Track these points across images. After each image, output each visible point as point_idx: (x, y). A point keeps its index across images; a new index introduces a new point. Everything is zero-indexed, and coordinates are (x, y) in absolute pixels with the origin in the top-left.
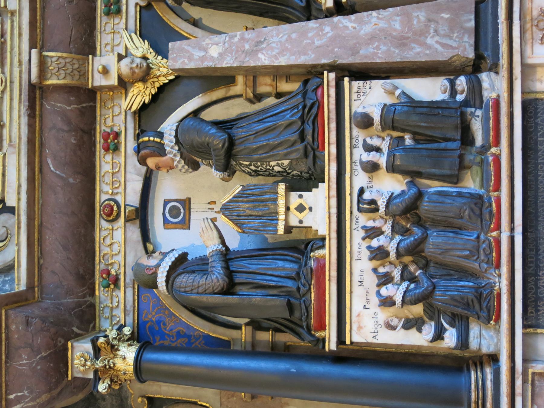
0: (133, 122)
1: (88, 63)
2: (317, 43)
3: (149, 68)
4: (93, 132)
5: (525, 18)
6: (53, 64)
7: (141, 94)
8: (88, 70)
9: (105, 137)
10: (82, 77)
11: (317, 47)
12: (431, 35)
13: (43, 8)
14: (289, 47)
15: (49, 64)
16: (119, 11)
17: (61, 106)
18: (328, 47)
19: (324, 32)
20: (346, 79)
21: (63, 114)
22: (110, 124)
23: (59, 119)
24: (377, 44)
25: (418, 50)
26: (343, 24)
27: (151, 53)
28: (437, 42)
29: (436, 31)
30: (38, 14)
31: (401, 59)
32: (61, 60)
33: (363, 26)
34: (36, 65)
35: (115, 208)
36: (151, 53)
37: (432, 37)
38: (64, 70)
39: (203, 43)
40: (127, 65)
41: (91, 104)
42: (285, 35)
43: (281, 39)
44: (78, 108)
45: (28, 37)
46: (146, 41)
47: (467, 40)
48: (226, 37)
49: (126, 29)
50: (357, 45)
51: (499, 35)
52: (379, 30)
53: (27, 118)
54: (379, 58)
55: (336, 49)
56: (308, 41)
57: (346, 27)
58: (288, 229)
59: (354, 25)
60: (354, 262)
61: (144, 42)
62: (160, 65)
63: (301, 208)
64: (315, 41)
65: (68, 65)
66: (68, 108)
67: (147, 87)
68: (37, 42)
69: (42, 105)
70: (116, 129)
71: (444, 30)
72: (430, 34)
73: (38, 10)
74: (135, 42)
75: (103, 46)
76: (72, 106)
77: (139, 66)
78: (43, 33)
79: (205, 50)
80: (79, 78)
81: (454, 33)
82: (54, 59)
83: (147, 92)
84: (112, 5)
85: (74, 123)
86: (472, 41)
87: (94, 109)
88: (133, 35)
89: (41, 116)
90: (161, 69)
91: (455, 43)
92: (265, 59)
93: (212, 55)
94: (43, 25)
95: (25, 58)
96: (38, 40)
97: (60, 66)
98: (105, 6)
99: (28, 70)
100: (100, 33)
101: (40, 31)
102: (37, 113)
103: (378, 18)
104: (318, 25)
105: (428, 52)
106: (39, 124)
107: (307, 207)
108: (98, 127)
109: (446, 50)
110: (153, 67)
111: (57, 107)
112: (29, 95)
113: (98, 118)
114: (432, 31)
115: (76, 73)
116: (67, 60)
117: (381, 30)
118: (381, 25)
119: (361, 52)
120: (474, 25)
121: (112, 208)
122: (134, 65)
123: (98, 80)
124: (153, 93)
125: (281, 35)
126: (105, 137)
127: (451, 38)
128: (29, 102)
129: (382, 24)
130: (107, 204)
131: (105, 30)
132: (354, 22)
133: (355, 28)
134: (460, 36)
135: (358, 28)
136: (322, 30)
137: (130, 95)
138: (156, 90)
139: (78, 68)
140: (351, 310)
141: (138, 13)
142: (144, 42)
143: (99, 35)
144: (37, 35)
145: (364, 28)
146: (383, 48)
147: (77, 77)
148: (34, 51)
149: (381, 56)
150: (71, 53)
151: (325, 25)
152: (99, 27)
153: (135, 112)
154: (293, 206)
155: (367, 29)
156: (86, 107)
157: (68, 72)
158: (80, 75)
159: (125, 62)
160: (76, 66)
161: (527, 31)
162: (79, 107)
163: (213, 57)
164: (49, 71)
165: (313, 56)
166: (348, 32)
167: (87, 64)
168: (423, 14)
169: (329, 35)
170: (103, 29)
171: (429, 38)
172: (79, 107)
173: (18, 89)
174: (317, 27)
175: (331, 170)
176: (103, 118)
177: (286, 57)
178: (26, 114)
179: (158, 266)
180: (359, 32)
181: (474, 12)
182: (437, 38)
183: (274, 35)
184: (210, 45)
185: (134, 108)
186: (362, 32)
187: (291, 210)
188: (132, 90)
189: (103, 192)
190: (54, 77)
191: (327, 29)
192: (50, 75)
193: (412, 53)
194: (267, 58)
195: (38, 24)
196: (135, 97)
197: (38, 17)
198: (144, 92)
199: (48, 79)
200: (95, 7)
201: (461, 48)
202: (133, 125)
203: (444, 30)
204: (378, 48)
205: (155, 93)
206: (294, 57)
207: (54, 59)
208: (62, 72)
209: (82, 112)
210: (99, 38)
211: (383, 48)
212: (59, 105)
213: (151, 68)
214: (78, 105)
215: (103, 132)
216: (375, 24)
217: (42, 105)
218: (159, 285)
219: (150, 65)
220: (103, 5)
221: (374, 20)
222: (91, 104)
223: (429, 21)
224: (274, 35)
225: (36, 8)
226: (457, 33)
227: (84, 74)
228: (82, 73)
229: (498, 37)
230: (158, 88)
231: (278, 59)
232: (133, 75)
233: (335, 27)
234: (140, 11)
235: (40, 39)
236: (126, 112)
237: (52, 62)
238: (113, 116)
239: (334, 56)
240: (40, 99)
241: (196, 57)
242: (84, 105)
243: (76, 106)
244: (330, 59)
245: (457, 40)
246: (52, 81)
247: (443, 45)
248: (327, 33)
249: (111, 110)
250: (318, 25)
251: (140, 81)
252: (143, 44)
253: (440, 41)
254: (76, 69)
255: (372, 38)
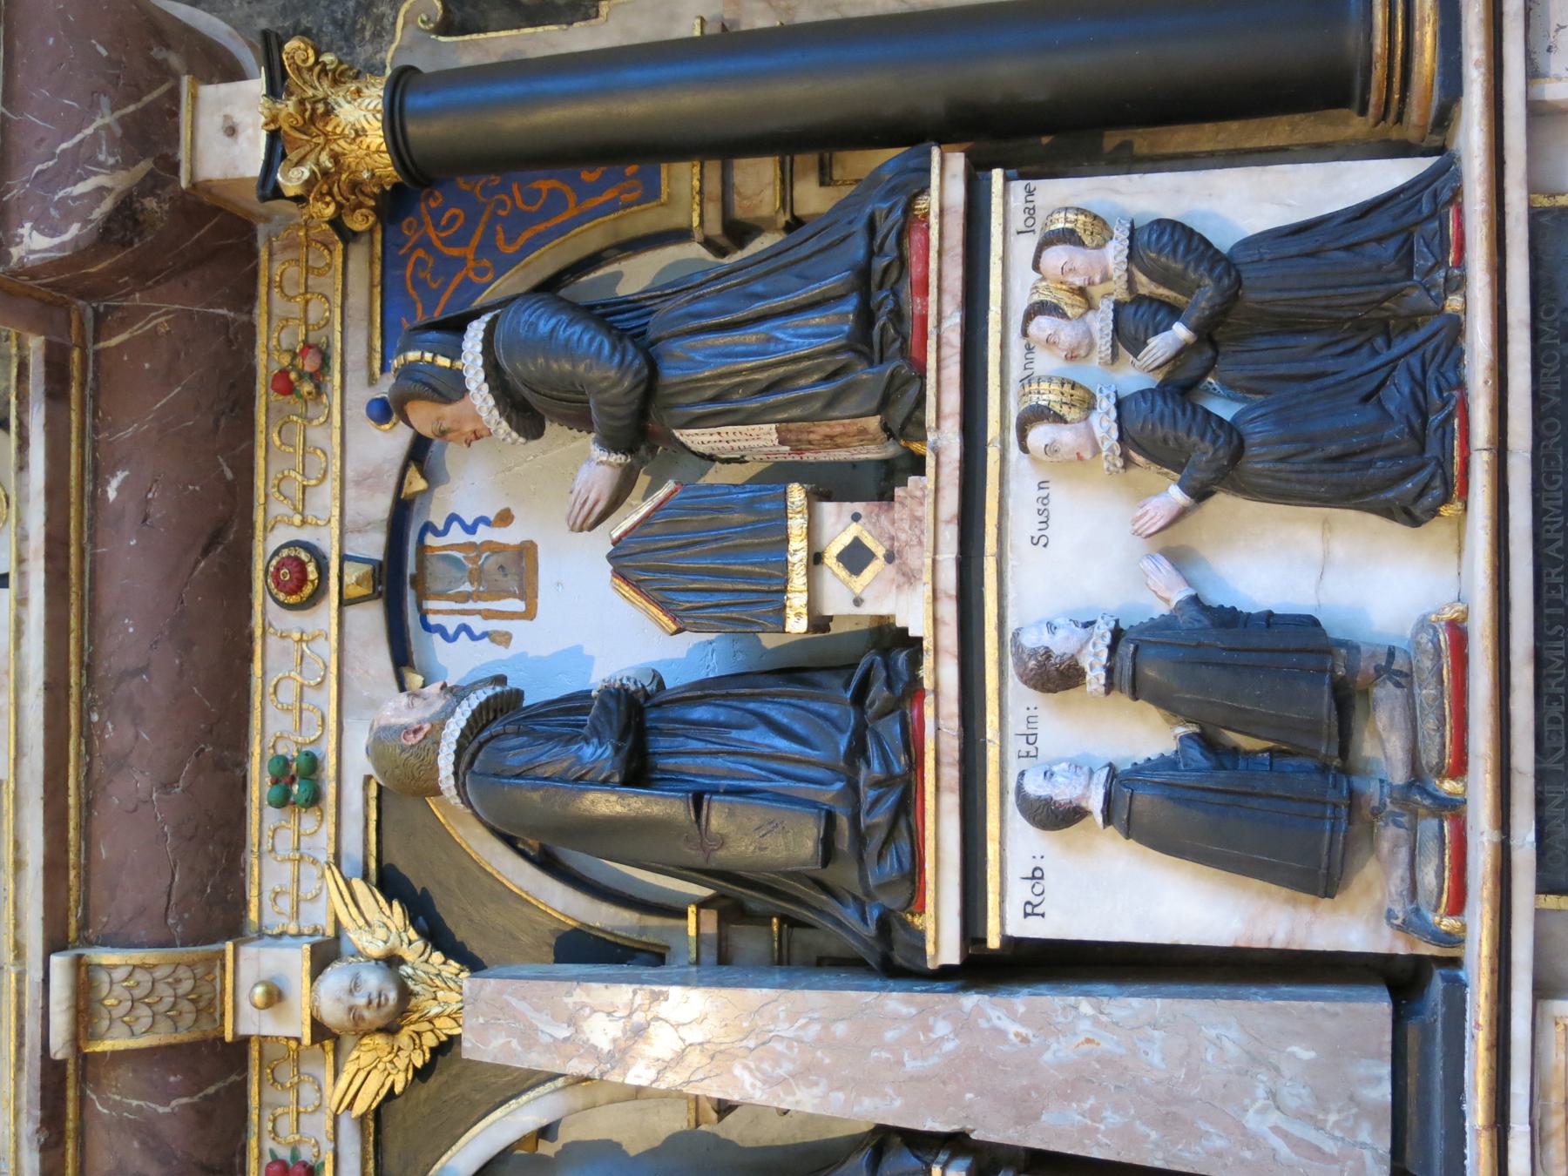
0: (357, 1137)
1: (223, 967)
2: (912, 1065)
3: (405, 994)
4: (237, 1161)
5: (1545, 1097)
6: (118, 990)
7: (381, 1066)
8: (223, 990)
9: (283, 774)
10: (204, 1014)
11: (911, 1078)
12: (1259, 1104)
13: (87, 806)
14: (827, 1061)
15: (105, 988)
16: (314, 799)
17: (140, 1107)
18: (944, 1083)
19: (933, 1036)
20: (997, 175)
21: (145, 1130)
22: (291, 1138)
23: (136, 1144)
24: (1092, 1101)
25: (1219, 1143)
26: (989, 1020)
27: (410, 943)
28: (1276, 1130)
29: (1272, 1095)
30: (72, 824)
31: (1167, 1162)
32: (140, 975)
33: (1052, 1040)
34: (65, 1006)
35: (312, 572)
36: (410, 943)
37: (1262, 1111)
38: (149, 1005)
39: (566, 1000)
40: (339, 1000)
41: (234, 1078)
42: (812, 1020)
43: (801, 1033)
44: (192, 1105)
45: (40, 913)
46: (396, 904)
47: (1369, 1141)
48: (635, 993)
49: (337, 856)
50: (1034, 1094)
51: (1467, 1151)
52: (1099, 1062)
53: (36, 1156)
54: (1099, 1144)
55: (969, 1096)
56: (885, 1055)
57: (1000, 1034)
58: (819, 623)
59: (1023, 1031)
60: (1013, 238)
61: (391, 906)
62: (438, 982)
63: (856, 557)
64: (906, 1058)
65: (161, 987)
66: (161, 1110)
67: (400, 1049)
68: (68, 909)
69: (82, 1100)
70: (307, 1154)
71: (1299, 1096)
72: (1254, 1101)
73: (72, 813)
74: (362, 905)
75: (267, 896)
76: (174, 1103)
77: (375, 1002)
78: (85, 881)
79: (572, 1021)
80: (196, 1021)
81: (1327, 1111)
82: (118, 975)
83: (401, 1063)
84: (293, 779)
85: (179, 1153)
86: (1385, 1145)
87: (241, 1091)
88: (358, 885)
89: (81, 1133)
90: (440, 994)
91: (1331, 1143)
92: (753, 1086)
93: (593, 1040)
94: (87, 858)
95: (34, 974)
96: (72, 904)
97: (138, 993)
98: (275, 782)
99: (40, 1012)
100: (260, 857)
101: (78, 876)
102: (70, 1125)
103: (1095, 1021)
104: (913, 1011)
105: (1248, 1154)
106: (75, 1156)
107: (880, 551)
108: (253, 1142)
109: (1304, 1161)
110: (417, 988)
111: (129, 1109)
112: (43, 1087)
113: (254, 1116)
114: (1261, 1092)
115: (185, 1006)
116: (158, 974)
117: (1106, 1061)
118: (1105, 1046)
119: (1044, 1118)
120: (1389, 1098)
121: (302, 566)
122: (361, 1001)
123: (253, 1022)
124: (419, 1064)
125: (802, 1021)
126: (283, 774)
127: (1319, 1127)
128: (43, 1106)
129: (1108, 1043)
130: (289, 557)
131: (273, 849)
132: (1022, 1020)
133: (1025, 1040)
134: (1349, 1124)
135: (1035, 1041)
136: (928, 1029)
137: (349, 1069)
138: (428, 1056)
139: (192, 991)
140: (1002, 843)
141: (373, 804)
142: (391, 906)
143: (256, 862)
144: (69, 889)
145: (1055, 1046)
146: (1113, 1119)
147: (189, 1018)
148: (57, 960)
149: (1105, 1140)
150: (168, 944)
151: (936, 1014)
152: (256, 840)
153: (362, 1118)
154: (833, 550)
155: (1059, 1052)
156: (217, 1092)
157: (162, 1008)
158: (198, 1011)
159: (335, 979)
160: (187, 985)
161: (1550, 1136)
162: (196, 1099)
163: (595, 1047)
164: (104, 1012)
165: (898, 1103)
166: (1005, 1048)
167: (218, 972)
168: (1234, 1033)
169: (949, 1046)
170: (267, 846)
171: (1251, 1111)
172: (196, 1099)
173: (13, 1025)
174: (910, 1018)
175: (946, 439)
176: (267, 1114)
177: (816, 1091)
178: (35, 1145)
179: (439, 723)
180: (1040, 1054)
181: (1389, 1058)
182: (1274, 1117)
183: (782, 1015)
184: (587, 1011)
185: (360, 1107)
186: (1048, 1057)
187: (827, 561)
188: (355, 1054)
189: (275, 728)
190: (120, 1028)
191: (942, 1028)
192: (105, 1023)
193: (1198, 1149)
194: (759, 1084)
195: (72, 856)
196: (362, 1075)
197: (72, 834)
198: (391, 1062)
199: (101, 1038)
200: (245, 777)
201: (1350, 1163)
202: (357, 1148)
203: (1299, 1096)
204: (1094, 1114)
205: (425, 1065)
206: (841, 1095)
207: (118, 975)
208: (144, 1011)
209: (204, 1114)
210: (256, 869)
211: (1113, 1119)
212: (135, 1103)
213: (412, 994)
214: (191, 1095)
215: (268, 1159)
216: (1088, 1041)
217: (82, 1100)
218: (443, 787)
219: (410, 983)
220: (268, 780)
221: (1084, 1026)
222: (234, 1078)
223: (1255, 1059)
224: (782, 1015)
225: (66, 807)
226: (1339, 1111)
227: (211, 1003)
228: (202, 1004)
229: (1464, 1157)
230: (432, 1050)
231: (794, 1094)
232: (356, 1024)
233: (964, 1025)
234: (379, 798)
235: (78, 902)
236: (336, 1118)
237: (111, 983)
238: (298, 1113)
239: (962, 1114)
240: (77, 1082)
241: (546, 1039)
242: (211, 1090)
243: (184, 1100)
244: (947, 1123)
245: (1338, 1133)
246: (112, 1042)
247: (1295, 1143)
248: (942, 1039)
249: (292, 1097)
250: (913, 1011)
251: (380, 1030)
252: (388, 912)
253: (1285, 1126)
254: (185, 996)
255: (1077, 1082)
